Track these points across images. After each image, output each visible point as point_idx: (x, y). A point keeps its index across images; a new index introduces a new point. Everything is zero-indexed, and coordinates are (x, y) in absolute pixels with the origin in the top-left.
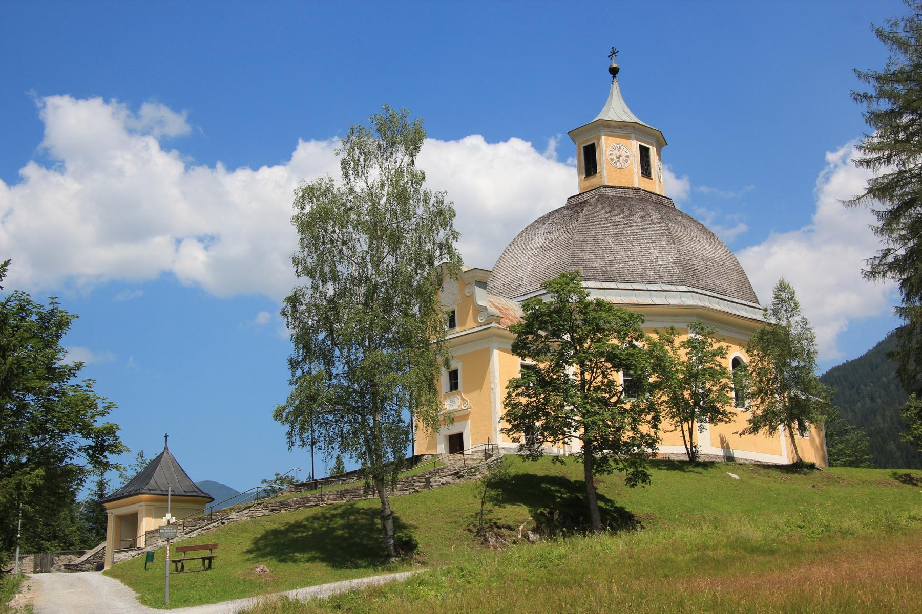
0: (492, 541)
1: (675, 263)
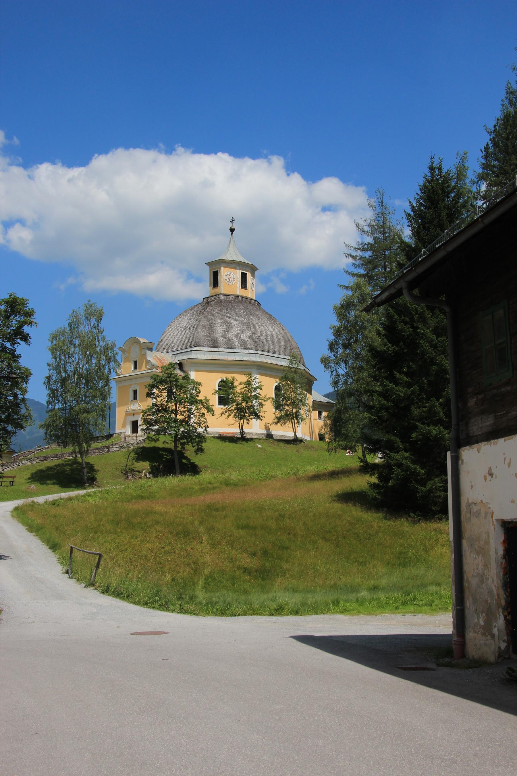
0: (130, 477)
1: (249, 338)
